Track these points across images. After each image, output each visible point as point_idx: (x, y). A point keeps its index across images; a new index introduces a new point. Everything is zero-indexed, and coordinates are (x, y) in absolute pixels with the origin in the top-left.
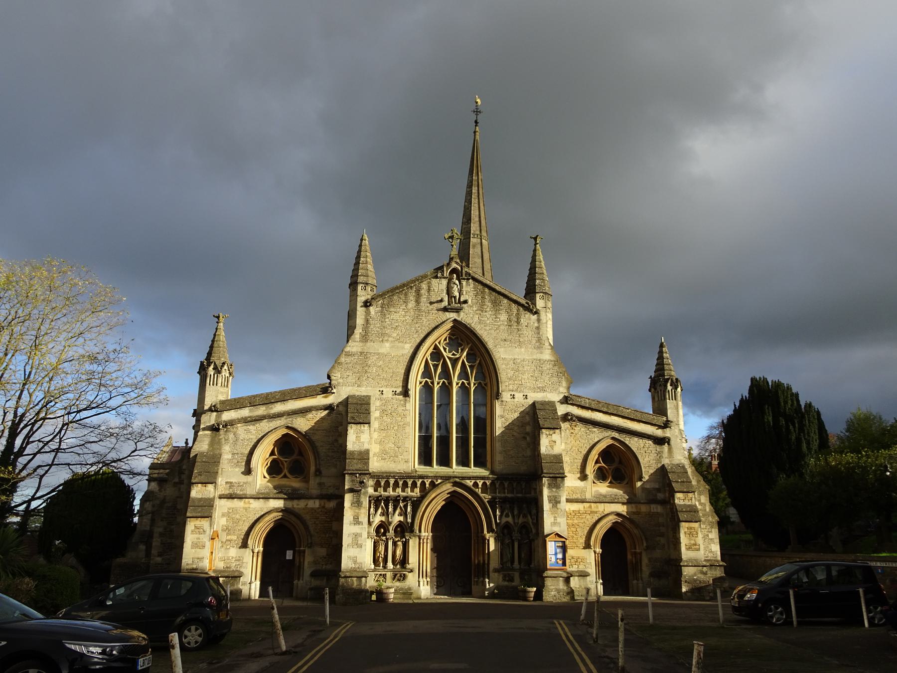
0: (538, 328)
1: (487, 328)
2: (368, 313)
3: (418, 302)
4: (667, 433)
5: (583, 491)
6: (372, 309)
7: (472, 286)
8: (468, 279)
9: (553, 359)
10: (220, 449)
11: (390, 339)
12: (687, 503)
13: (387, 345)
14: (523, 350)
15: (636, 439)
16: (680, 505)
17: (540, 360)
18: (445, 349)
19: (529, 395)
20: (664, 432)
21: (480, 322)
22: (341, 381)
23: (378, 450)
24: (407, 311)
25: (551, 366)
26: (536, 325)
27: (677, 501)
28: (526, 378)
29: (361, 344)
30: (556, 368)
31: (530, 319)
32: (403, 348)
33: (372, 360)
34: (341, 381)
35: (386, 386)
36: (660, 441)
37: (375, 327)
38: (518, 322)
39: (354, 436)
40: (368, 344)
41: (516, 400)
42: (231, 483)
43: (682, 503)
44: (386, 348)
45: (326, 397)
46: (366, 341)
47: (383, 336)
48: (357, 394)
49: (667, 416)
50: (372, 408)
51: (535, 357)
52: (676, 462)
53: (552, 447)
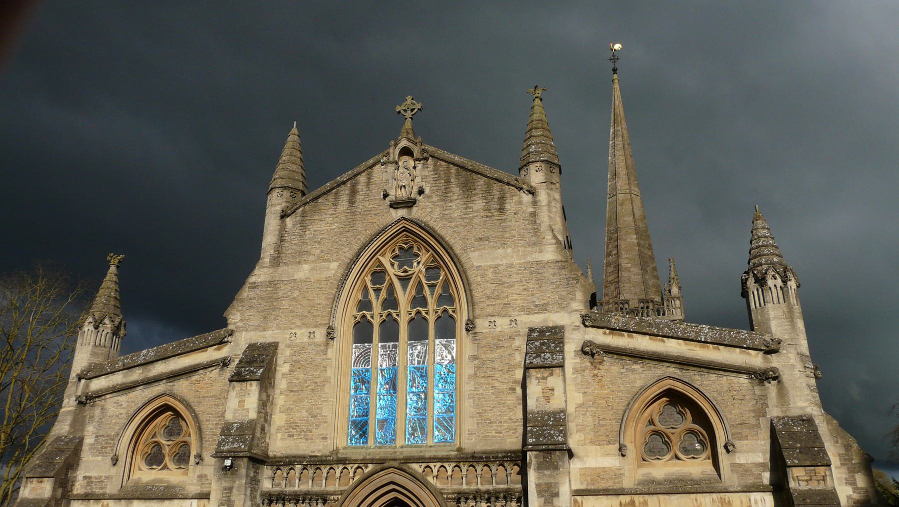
0: (534, 214)
1: (453, 225)
2: (283, 228)
3: (352, 202)
4: (775, 361)
5: (618, 474)
6: (289, 221)
7: (431, 168)
8: (426, 159)
9: (560, 258)
10: (83, 430)
11: (311, 258)
12: (814, 486)
13: (306, 267)
14: (509, 250)
15: (713, 377)
16: (795, 490)
17: (537, 263)
18: (392, 265)
19: (518, 318)
20: (766, 361)
21: (443, 217)
22: (240, 324)
23: (283, 423)
24: (335, 216)
25: (556, 271)
26: (531, 210)
27: (792, 484)
28: (516, 295)
29: (271, 270)
30: (564, 272)
31: (520, 203)
32: (328, 269)
33: (284, 290)
34: (240, 324)
35: (299, 327)
36: (763, 377)
37: (290, 247)
38: (501, 210)
39: (237, 400)
40: (282, 268)
41: (498, 329)
42: (90, 478)
43: (803, 486)
44: (303, 271)
45: (218, 349)
46: (278, 266)
47: (301, 255)
48: (261, 340)
49: (771, 333)
50: (280, 360)
51: (529, 259)
52: (795, 412)
53: (548, 399)
